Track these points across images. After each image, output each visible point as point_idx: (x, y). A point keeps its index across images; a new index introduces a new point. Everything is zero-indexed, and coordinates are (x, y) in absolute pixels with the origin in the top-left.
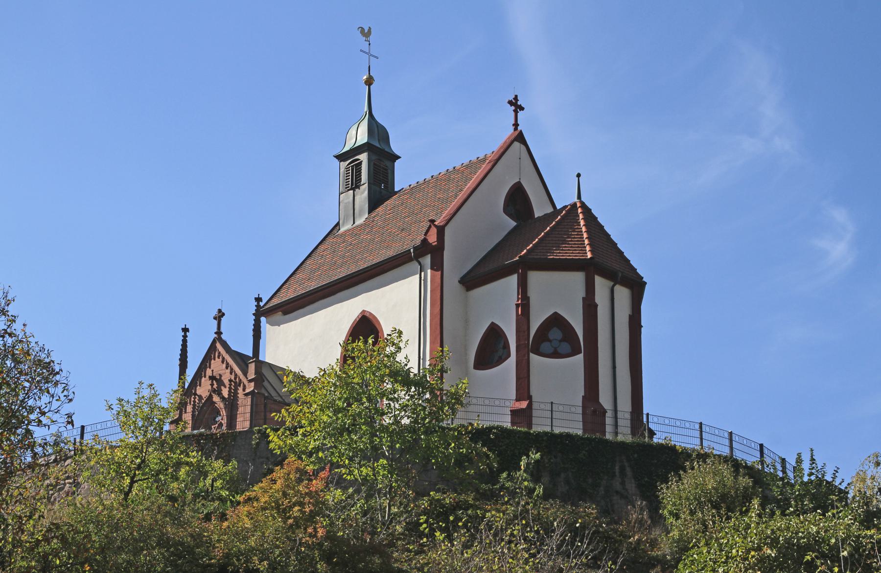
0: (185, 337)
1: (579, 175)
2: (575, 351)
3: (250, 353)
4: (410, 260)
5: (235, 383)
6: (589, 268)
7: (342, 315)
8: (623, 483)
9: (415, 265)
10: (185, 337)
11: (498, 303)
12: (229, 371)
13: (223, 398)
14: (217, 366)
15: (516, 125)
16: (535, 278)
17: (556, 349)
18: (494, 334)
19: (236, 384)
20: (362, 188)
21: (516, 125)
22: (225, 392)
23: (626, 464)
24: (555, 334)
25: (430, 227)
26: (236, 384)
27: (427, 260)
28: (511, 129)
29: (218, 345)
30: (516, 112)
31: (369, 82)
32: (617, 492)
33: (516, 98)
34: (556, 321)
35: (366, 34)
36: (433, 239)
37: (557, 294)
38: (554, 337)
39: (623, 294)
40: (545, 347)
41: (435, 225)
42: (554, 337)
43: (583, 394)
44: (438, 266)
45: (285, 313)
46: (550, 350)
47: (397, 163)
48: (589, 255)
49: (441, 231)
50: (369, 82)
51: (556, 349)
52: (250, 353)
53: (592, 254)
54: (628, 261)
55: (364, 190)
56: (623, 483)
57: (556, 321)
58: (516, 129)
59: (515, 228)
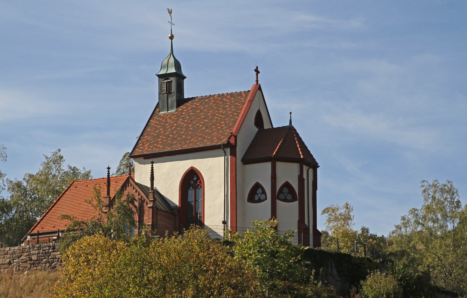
0: (109, 171)
1: (291, 113)
2: (294, 199)
3: (149, 185)
4: (221, 148)
5: (142, 200)
6: (302, 162)
7: (181, 167)
8: (332, 270)
9: (221, 151)
10: (109, 171)
11: (261, 173)
12: (137, 193)
13: (135, 206)
14: (129, 190)
15: (257, 81)
16: (279, 165)
17: (283, 193)
18: (257, 186)
19: (142, 202)
20: (172, 94)
21: (257, 81)
22: (137, 204)
23: (333, 262)
24: (286, 190)
25: (231, 136)
26: (142, 202)
27: (228, 150)
28: (255, 83)
29: (131, 180)
30: (257, 74)
31: (172, 38)
32: (330, 274)
33: (257, 67)
34: (287, 185)
35: (170, 12)
36: (232, 141)
37: (288, 173)
38: (285, 193)
39: (311, 171)
40: (282, 196)
41: (233, 135)
42: (285, 193)
43: (298, 219)
44: (233, 154)
45: (145, 158)
46: (283, 198)
47: (185, 80)
48: (302, 157)
49: (236, 137)
50: (172, 38)
51: (283, 193)
52: (149, 185)
53: (303, 156)
54: (312, 156)
55: (174, 95)
56: (332, 270)
57: (287, 185)
58: (257, 83)
59: (258, 132)
